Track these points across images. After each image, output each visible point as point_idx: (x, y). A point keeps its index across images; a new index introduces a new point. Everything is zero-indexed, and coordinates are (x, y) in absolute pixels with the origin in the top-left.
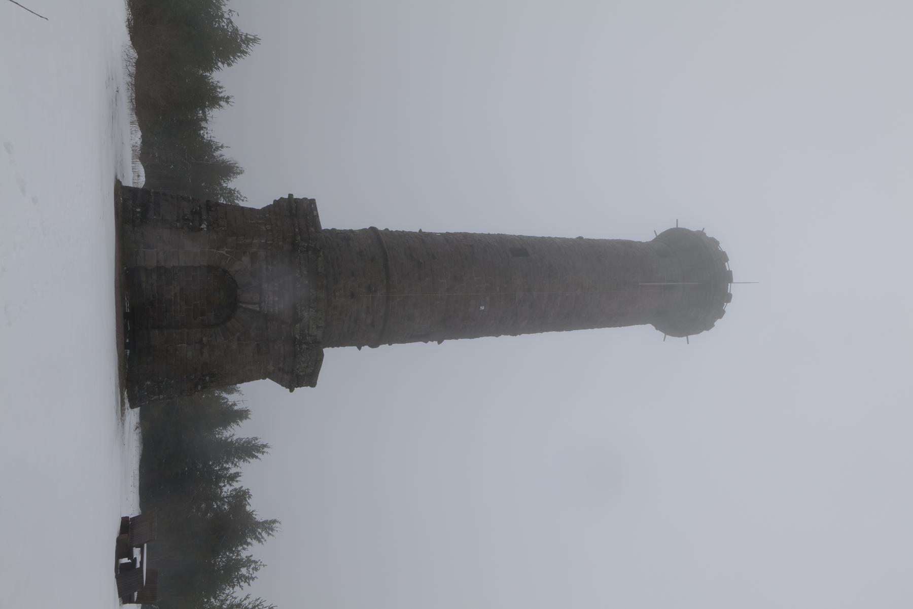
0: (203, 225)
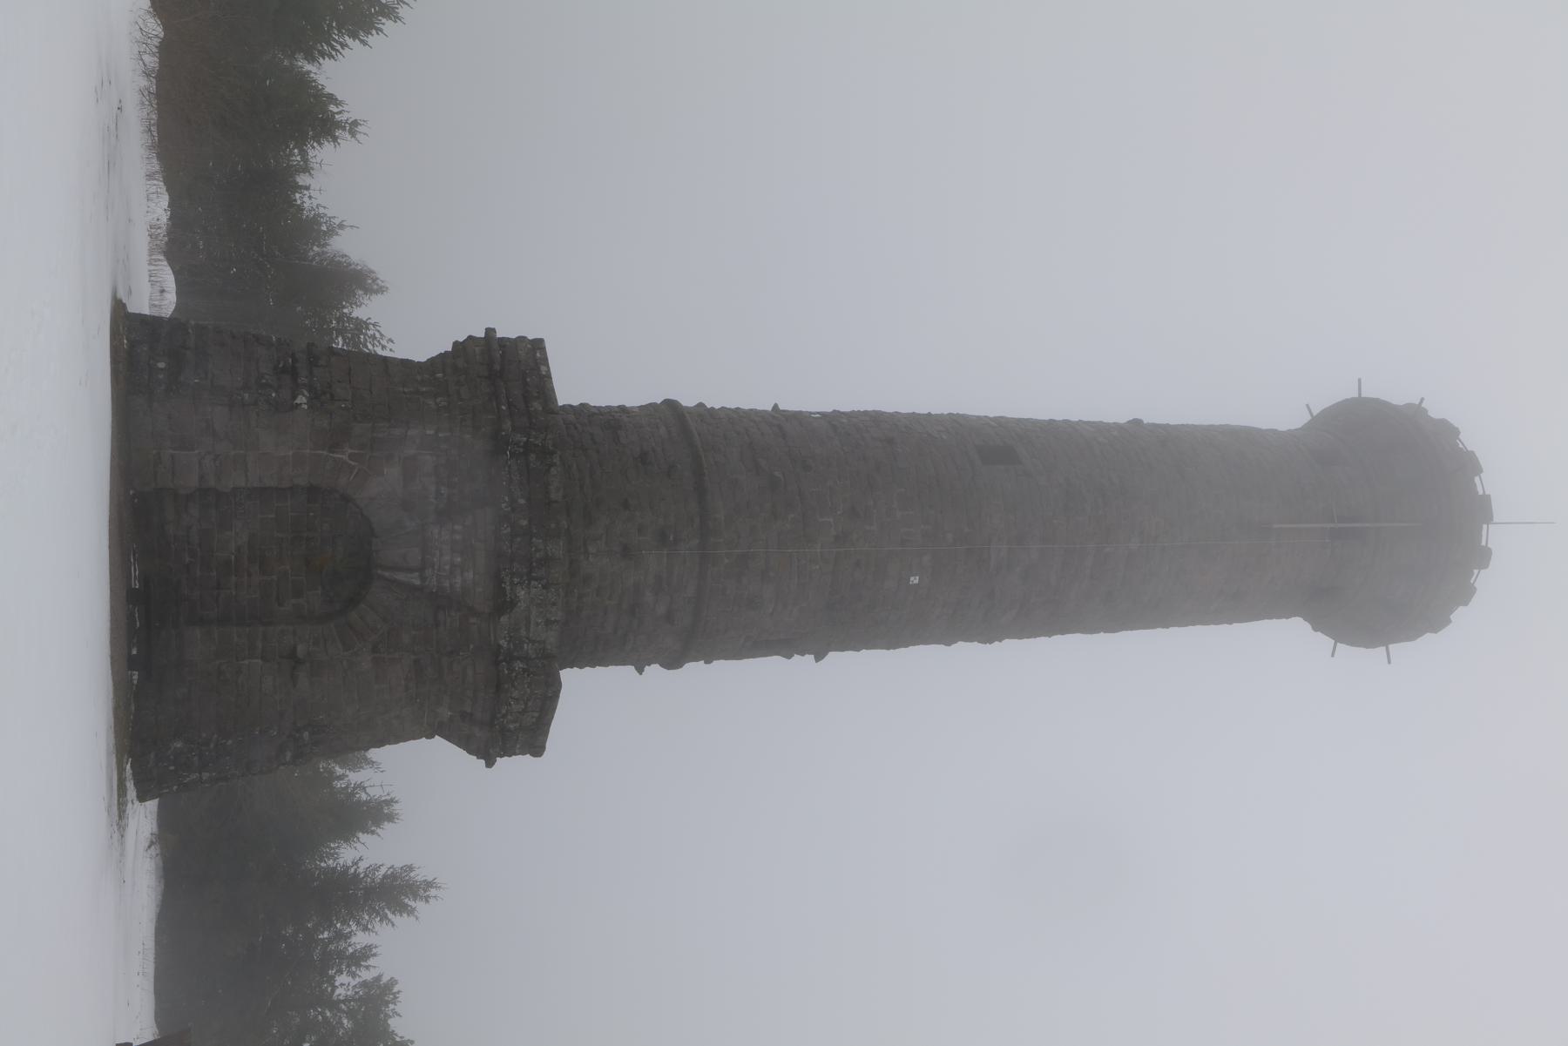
0: (300, 396)
